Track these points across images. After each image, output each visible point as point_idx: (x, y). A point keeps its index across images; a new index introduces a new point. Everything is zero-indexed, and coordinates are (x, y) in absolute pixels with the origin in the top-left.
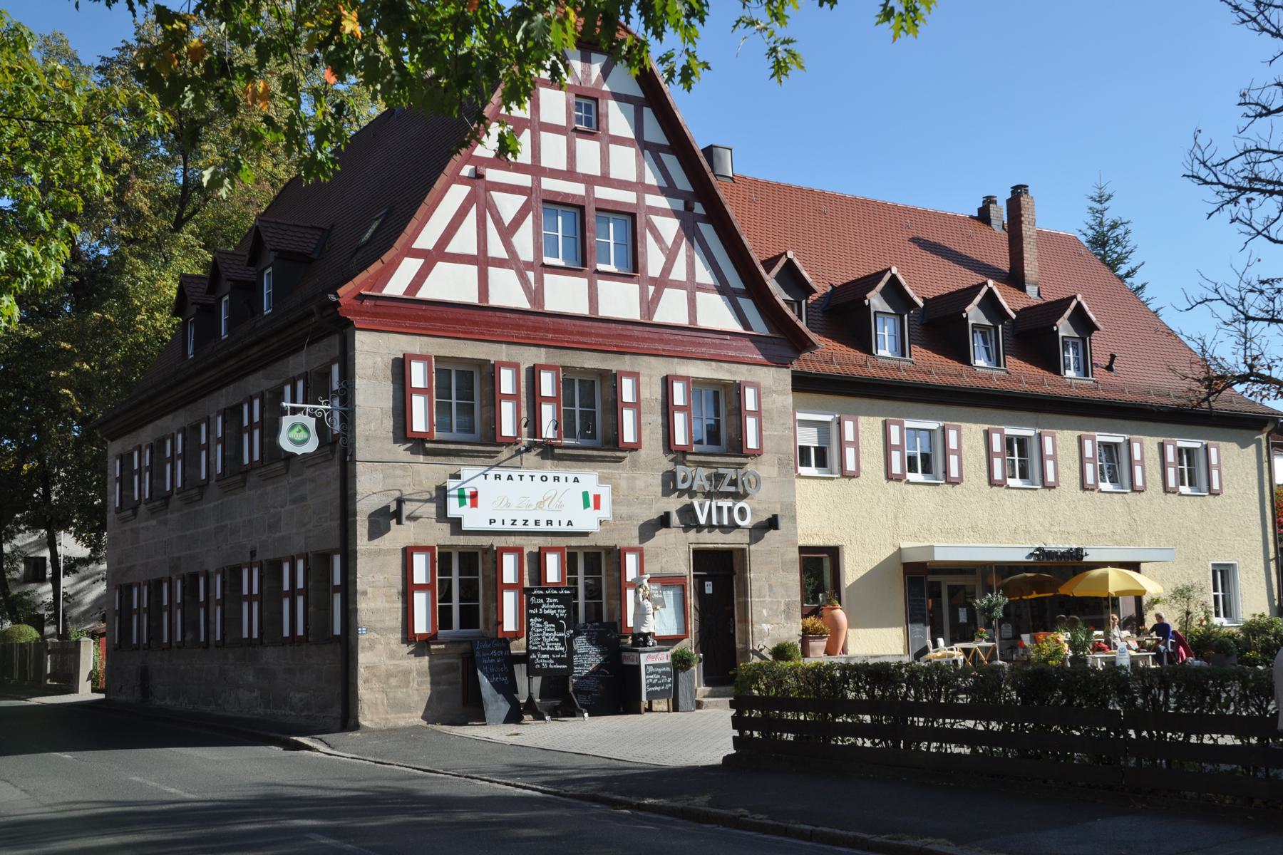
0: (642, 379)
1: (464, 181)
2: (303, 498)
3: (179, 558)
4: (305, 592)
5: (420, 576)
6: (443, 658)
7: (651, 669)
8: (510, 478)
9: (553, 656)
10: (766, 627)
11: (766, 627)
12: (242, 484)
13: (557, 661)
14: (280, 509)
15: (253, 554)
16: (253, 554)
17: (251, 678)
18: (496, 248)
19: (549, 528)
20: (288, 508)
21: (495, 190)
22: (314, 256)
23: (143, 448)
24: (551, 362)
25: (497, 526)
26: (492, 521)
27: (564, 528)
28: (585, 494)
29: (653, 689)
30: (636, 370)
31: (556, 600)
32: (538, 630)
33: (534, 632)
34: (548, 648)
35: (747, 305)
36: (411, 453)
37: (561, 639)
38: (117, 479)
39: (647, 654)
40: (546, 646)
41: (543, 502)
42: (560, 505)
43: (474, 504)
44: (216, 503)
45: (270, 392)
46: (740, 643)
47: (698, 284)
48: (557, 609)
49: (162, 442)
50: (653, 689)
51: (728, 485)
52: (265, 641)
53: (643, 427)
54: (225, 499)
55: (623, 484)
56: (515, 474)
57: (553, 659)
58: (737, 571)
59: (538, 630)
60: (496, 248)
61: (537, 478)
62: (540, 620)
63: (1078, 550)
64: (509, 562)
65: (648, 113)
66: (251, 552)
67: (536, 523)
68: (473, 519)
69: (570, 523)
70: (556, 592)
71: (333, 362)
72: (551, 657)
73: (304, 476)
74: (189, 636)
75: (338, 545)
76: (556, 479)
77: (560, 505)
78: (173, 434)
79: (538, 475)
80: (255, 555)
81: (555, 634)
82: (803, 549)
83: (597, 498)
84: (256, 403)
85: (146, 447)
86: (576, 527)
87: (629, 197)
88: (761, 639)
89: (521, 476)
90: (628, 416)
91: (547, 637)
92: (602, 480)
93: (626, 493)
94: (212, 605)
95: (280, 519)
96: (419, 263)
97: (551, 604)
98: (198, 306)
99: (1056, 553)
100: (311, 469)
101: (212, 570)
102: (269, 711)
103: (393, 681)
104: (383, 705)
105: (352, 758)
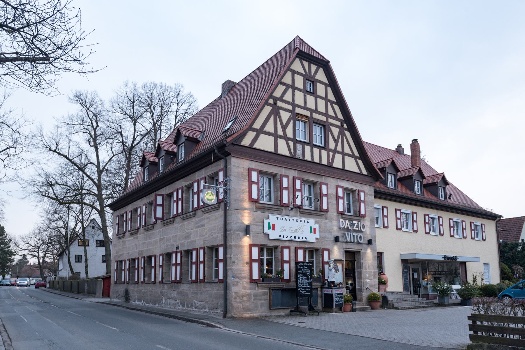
0: (329, 186)
1: (270, 105)
2: (203, 225)
3: (143, 251)
4: (180, 264)
5: (255, 256)
6: (262, 290)
7: (337, 296)
8: (286, 219)
9: (306, 290)
10: (368, 280)
11: (368, 280)
12: (173, 222)
13: (308, 292)
14: (191, 230)
15: (177, 248)
16: (177, 248)
17: (175, 295)
18: (280, 132)
19: (299, 240)
20: (195, 229)
21: (281, 110)
22: (200, 140)
23: (128, 212)
24: (299, 176)
25: (281, 238)
26: (280, 236)
27: (304, 240)
28: (311, 227)
29: (337, 303)
30: (326, 182)
31: (307, 268)
32: (301, 279)
33: (300, 280)
34: (304, 286)
35: (360, 162)
36: (411, 144)
37: (308, 283)
38: (117, 224)
39: (335, 289)
40: (303, 286)
41: (297, 230)
42: (303, 231)
43: (274, 229)
44: (160, 230)
45: (186, 187)
46: (358, 286)
47: (345, 153)
48: (307, 271)
49: (136, 210)
50: (337, 303)
51: (356, 227)
52: (183, 281)
53: (329, 204)
54: (164, 228)
55: (322, 224)
56: (287, 218)
57: (306, 291)
58: (357, 260)
59: (301, 279)
60: (280, 132)
61: (295, 220)
62: (301, 275)
63: (456, 257)
64: (286, 252)
65: (329, 89)
66: (176, 247)
67: (295, 237)
68: (274, 235)
69: (306, 238)
70: (307, 264)
71: (220, 170)
72: (305, 290)
73: (203, 217)
74: (146, 279)
75: (222, 243)
76: (301, 221)
77: (303, 231)
78: (141, 206)
79: (295, 219)
80: (178, 248)
81: (306, 281)
82: (378, 253)
83: (315, 229)
84: (180, 191)
85: (129, 212)
86: (308, 240)
87: (323, 118)
88: (366, 285)
89: (290, 219)
90: (325, 199)
91: (304, 282)
92: (316, 223)
93: (323, 228)
94: (157, 268)
95: (191, 233)
96: (254, 134)
97: (305, 269)
98: (150, 162)
99: (449, 257)
100: (207, 214)
101: (158, 254)
102: (184, 308)
103: (245, 299)
104: (241, 308)
105: (247, 334)
